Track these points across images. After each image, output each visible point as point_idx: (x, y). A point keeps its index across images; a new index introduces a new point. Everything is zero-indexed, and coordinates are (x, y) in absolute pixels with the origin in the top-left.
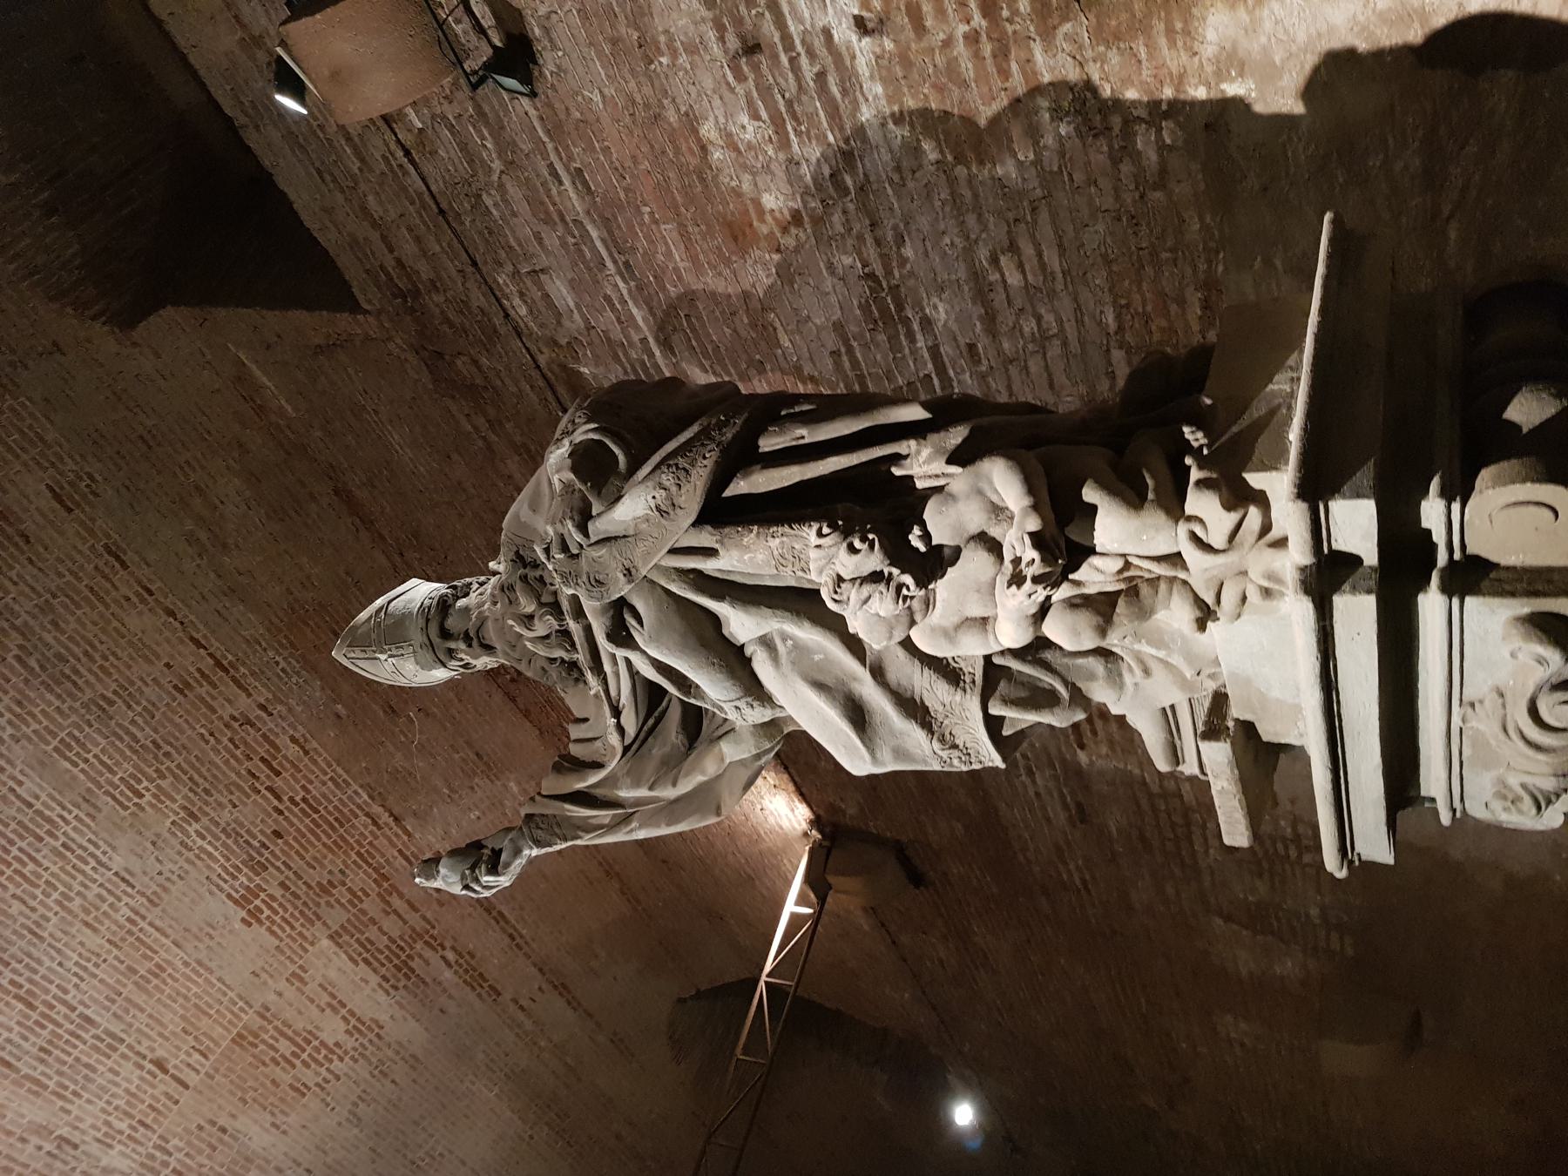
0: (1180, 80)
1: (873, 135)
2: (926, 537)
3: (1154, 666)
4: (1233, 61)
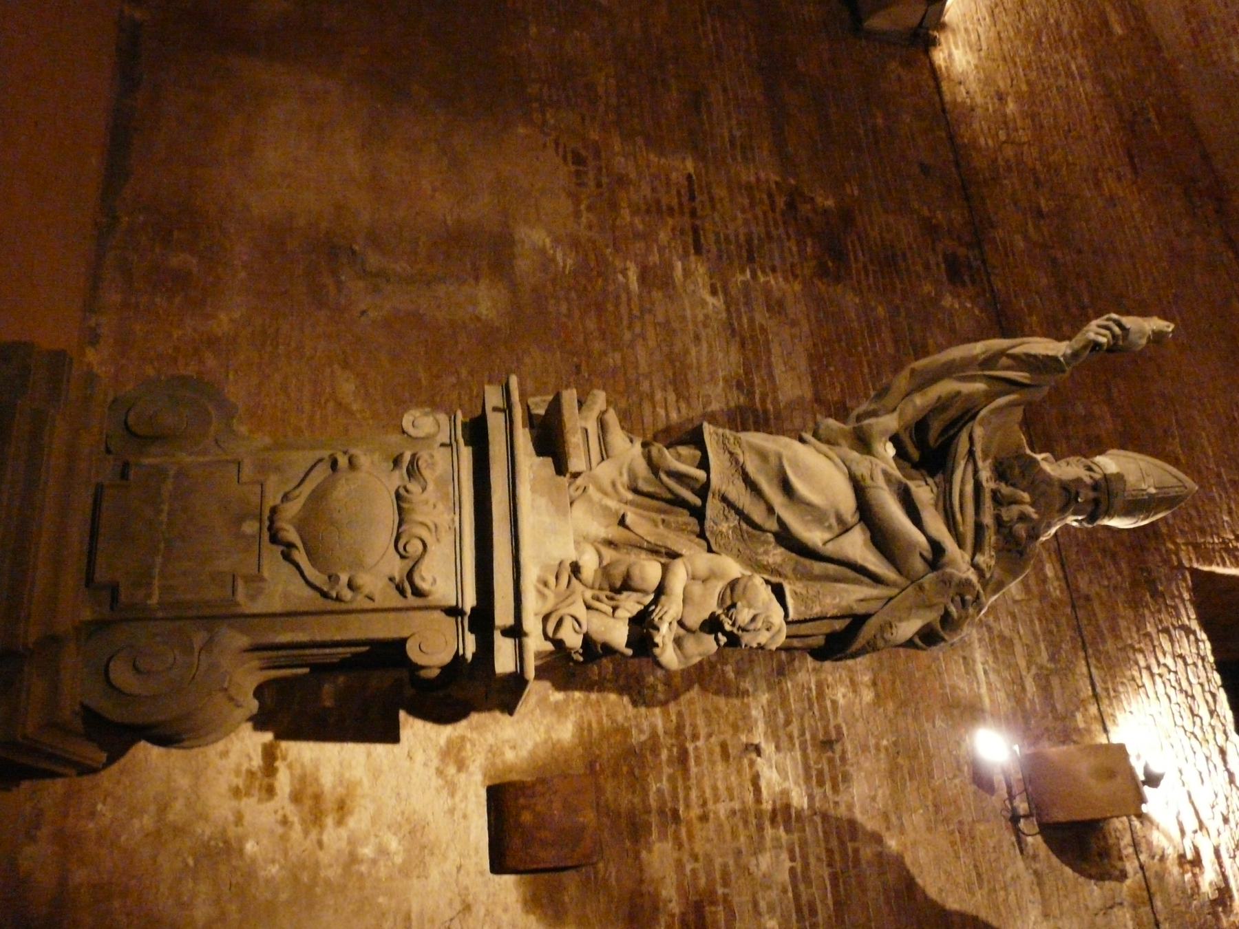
0: (587, 702)
1: (763, 685)
2: (717, 639)
3: (609, 489)
4: (559, 710)
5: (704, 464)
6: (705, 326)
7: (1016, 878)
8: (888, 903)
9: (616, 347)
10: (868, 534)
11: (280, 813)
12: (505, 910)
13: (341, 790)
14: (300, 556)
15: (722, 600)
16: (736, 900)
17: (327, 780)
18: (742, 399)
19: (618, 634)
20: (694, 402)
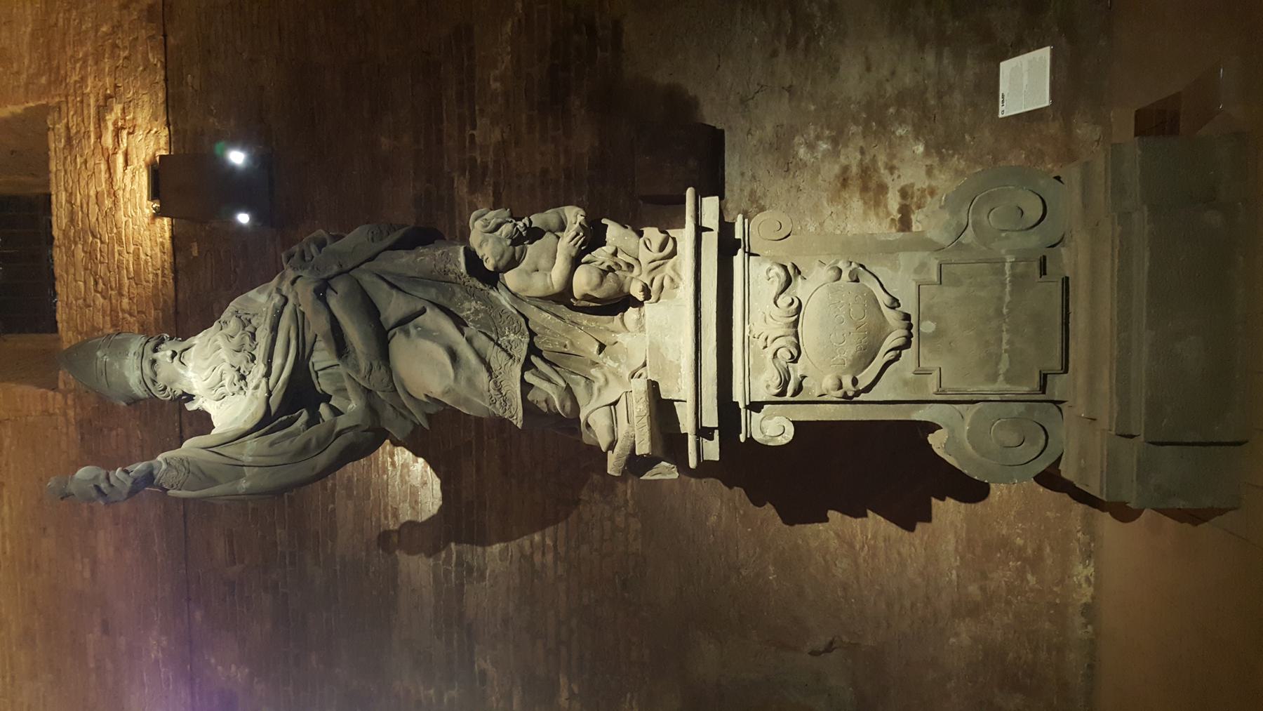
3: (610, 377)
5: (526, 387)
10: (382, 318)
11: (895, 176)
13: (845, 195)
14: (883, 299)
15: (523, 252)
17: (856, 204)
19: (613, 231)
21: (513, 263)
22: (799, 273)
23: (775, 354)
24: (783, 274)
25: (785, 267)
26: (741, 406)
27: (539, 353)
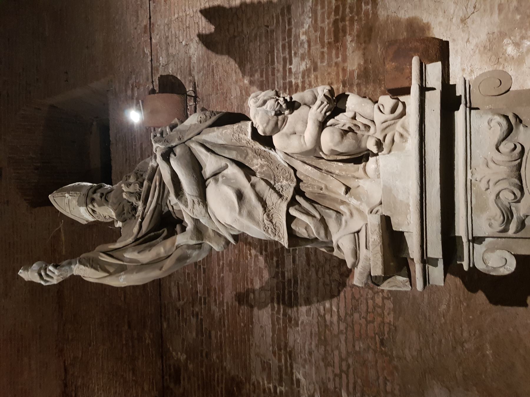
3: (355, 212)
5: (290, 219)
6: (305, 360)
7: (199, 72)
8: (251, 55)
9: (358, 353)
10: (203, 172)
12: (440, 23)
15: (284, 120)
16: (319, 46)
18: (290, 311)
19: (353, 102)
20: (316, 314)
21: (276, 128)
22: (521, 121)
23: (498, 195)
24: (504, 123)
25: (506, 117)
26: (465, 240)
27: (302, 194)
